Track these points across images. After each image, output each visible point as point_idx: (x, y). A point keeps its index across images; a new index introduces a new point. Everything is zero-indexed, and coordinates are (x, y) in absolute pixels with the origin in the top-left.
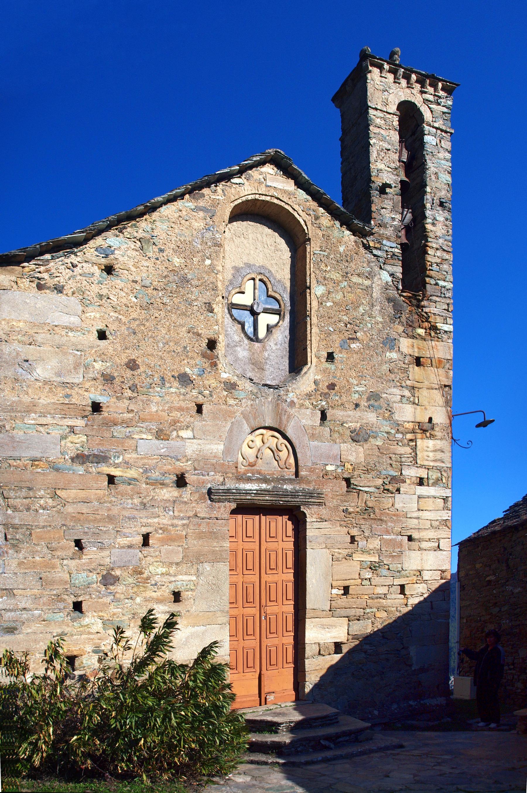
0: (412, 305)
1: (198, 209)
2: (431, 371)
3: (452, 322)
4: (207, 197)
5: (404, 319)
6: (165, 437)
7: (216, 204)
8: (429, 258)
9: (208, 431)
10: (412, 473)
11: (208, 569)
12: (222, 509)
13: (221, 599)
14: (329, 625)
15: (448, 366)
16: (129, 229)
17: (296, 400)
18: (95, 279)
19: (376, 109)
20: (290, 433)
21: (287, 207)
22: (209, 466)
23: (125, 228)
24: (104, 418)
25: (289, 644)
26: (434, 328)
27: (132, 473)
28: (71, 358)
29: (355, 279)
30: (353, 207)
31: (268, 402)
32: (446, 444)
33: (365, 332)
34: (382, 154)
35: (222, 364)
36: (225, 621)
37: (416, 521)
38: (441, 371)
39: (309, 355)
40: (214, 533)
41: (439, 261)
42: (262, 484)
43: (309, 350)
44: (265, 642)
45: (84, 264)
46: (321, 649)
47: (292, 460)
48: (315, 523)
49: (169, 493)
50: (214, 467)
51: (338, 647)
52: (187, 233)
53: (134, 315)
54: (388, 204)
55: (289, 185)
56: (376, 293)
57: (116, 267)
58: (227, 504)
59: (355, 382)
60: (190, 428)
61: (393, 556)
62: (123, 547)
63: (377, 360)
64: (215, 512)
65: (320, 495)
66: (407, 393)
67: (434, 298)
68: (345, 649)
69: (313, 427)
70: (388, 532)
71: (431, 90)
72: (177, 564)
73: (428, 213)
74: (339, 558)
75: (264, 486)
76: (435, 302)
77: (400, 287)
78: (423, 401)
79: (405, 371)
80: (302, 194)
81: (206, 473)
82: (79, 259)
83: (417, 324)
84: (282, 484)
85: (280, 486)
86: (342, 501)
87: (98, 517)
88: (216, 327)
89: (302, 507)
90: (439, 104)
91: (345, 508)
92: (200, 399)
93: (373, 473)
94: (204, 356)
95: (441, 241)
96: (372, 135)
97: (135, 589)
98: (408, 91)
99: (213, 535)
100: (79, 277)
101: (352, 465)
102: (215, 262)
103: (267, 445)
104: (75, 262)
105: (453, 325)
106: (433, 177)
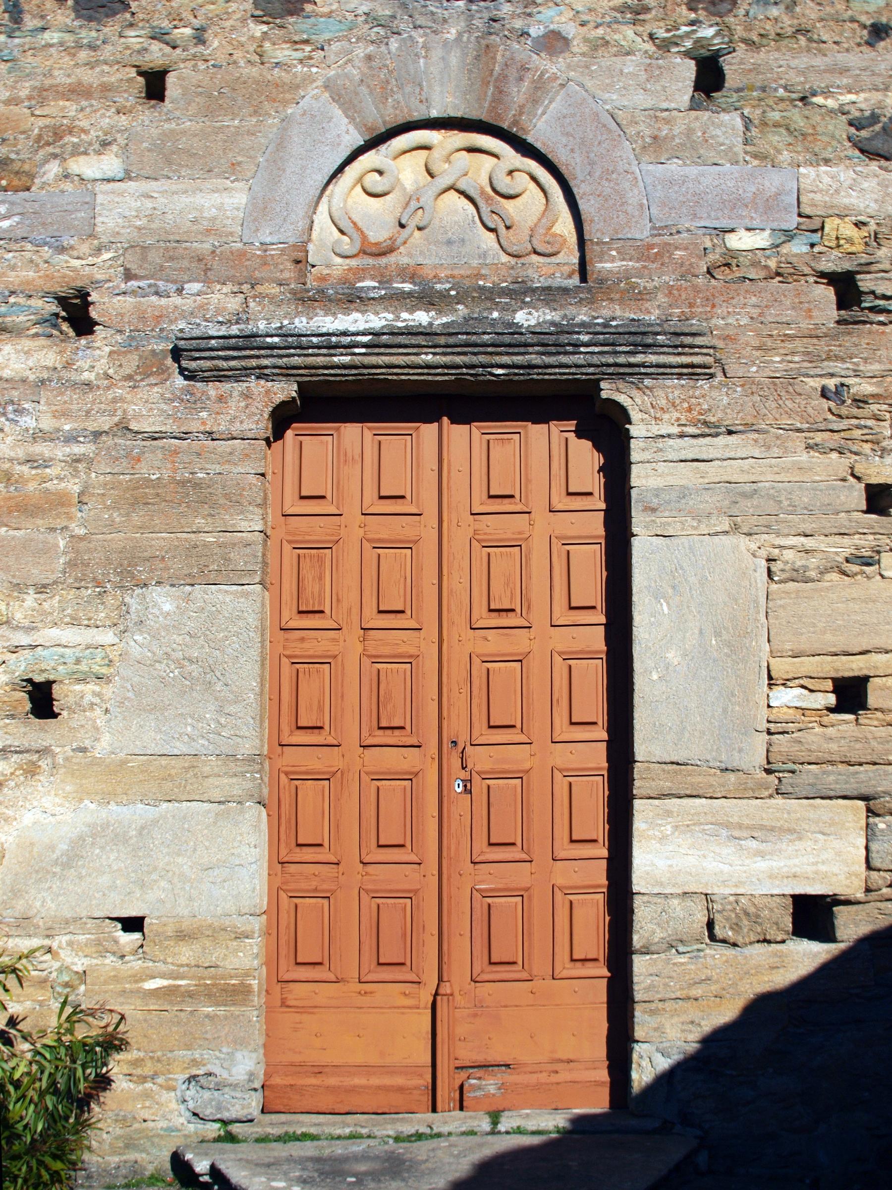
6: (16, 182)
9: (186, 151)
11: (167, 607)
12: (235, 404)
13: (220, 711)
14: (762, 828)
20: (538, 133)
22: (185, 263)
25: (589, 889)
31: (446, 42)
36: (237, 791)
40: (197, 485)
42: (411, 310)
44: (466, 881)
46: (718, 917)
47: (565, 226)
48: (671, 442)
50: (205, 269)
51: (812, 915)
58: (255, 386)
60: (114, 148)
64: (204, 414)
65: (688, 340)
68: (851, 927)
72: (42, 589)
74: (806, 568)
75: (422, 318)
81: (172, 287)
84: (504, 309)
85: (495, 315)
89: (603, 385)
91: (831, 383)
92: (157, 55)
99: (195, 493)
101: (859, 225)
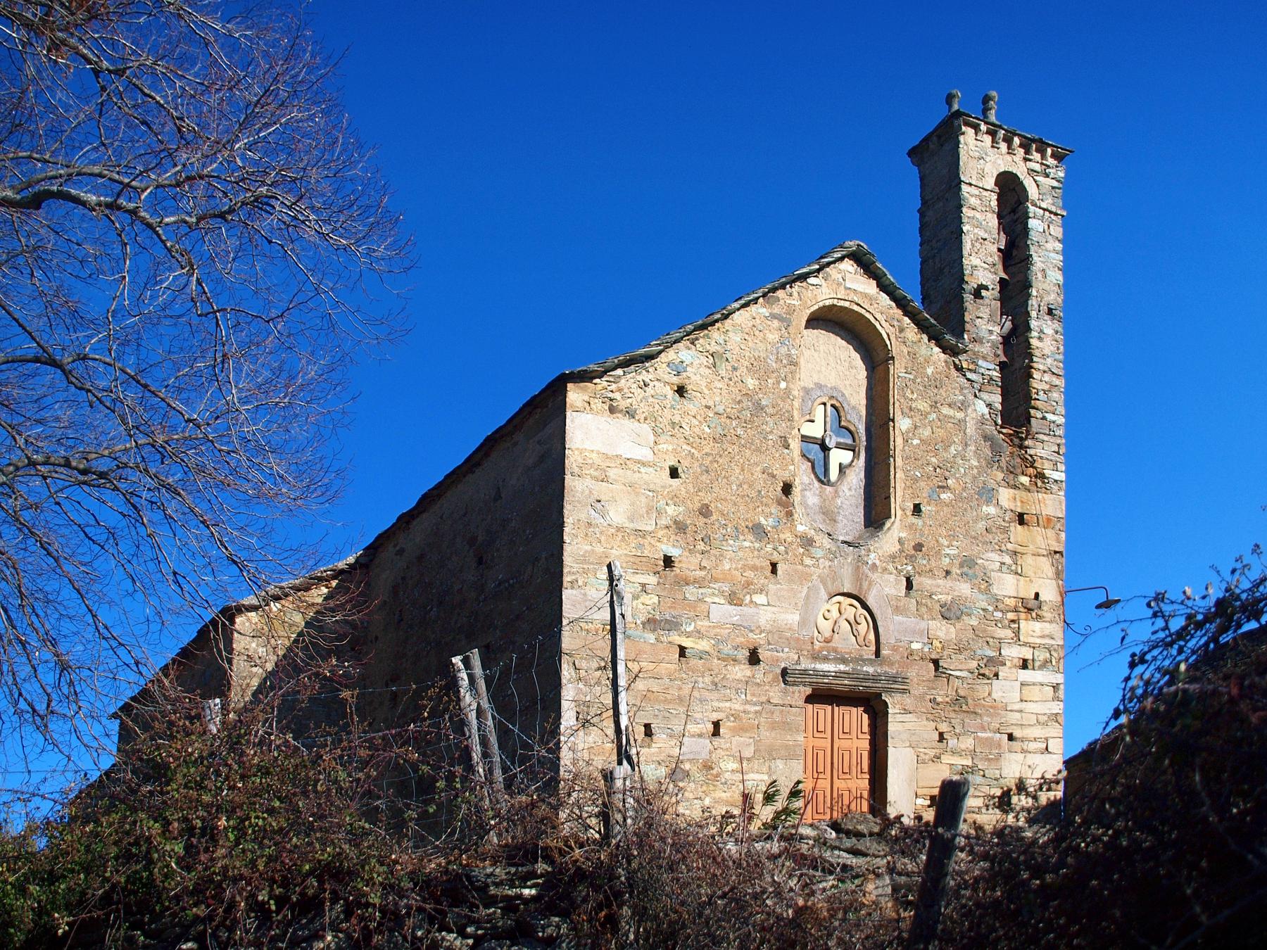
0: (1014, 446)
1: (774, 316)
2: (1037, 532)
3: (1064, 468)
4: (782, 302)
5: (1003, 464)
7: (791, 310)
8: (1034, 384)
10: (1013, 653)
12: (797, 694)
15: (1058, 526)
16: (701, 341)
17: (878, 562)
18: (668, 403)
19: (971, 185)
20: (871, 602)
21: (867, 315)
23: (697, 339)
24: (676, 576)
26: (1041, 476)
27: (704, 645)
28: (643, 500)
29: (946, 410)
30: (941, 312)
32: (1056, 629)
33: (957, 479)
34: (977, 244)
35: (799, 512)
37: (1018, 715)
38: (1050, 533)
39: (893, 506)
41: (1046, 387)
43: (892, 500)
45: (656, 383)
47: (872, 636)
49: (742, 671)
52: (762, 346)
53: (707, 450)
54: (984, 312)
55: (870, 287)
56: (971, 429)
57: (689, 387)
58: (801, 688)
59: (946, 543)
61: (989, 760)
62: (693, 736)
63: (971, 515)
66: (1008, 560)
67: (1041, 437)
69: (898, 598)
70: (983, 729)
71: (1037, 156)
73: (1034, 324)
75: (842, 667)
76: (1043, 442)
77: (1000, 422)
78: (1028, 571)
79: (1006, 531)
80: (884, 298)
82: (650, 377)
83: (1019, 471)
86: (929, 689)
87: (669, 697)
88: (792, 468)
90: (1047, 176)
92: (776, 557)
93: (966, 653)
94: (779, 503)
95: (1049, 361)
96: (965, 220)
97: (704, 788)
98: (1009, 158)
99: (785, 726)
100: (651, 400)
102: (792, 386)
103: (844, 616)
104: (647, 380)
105: (1066, 472)
106: (1039, 275)
